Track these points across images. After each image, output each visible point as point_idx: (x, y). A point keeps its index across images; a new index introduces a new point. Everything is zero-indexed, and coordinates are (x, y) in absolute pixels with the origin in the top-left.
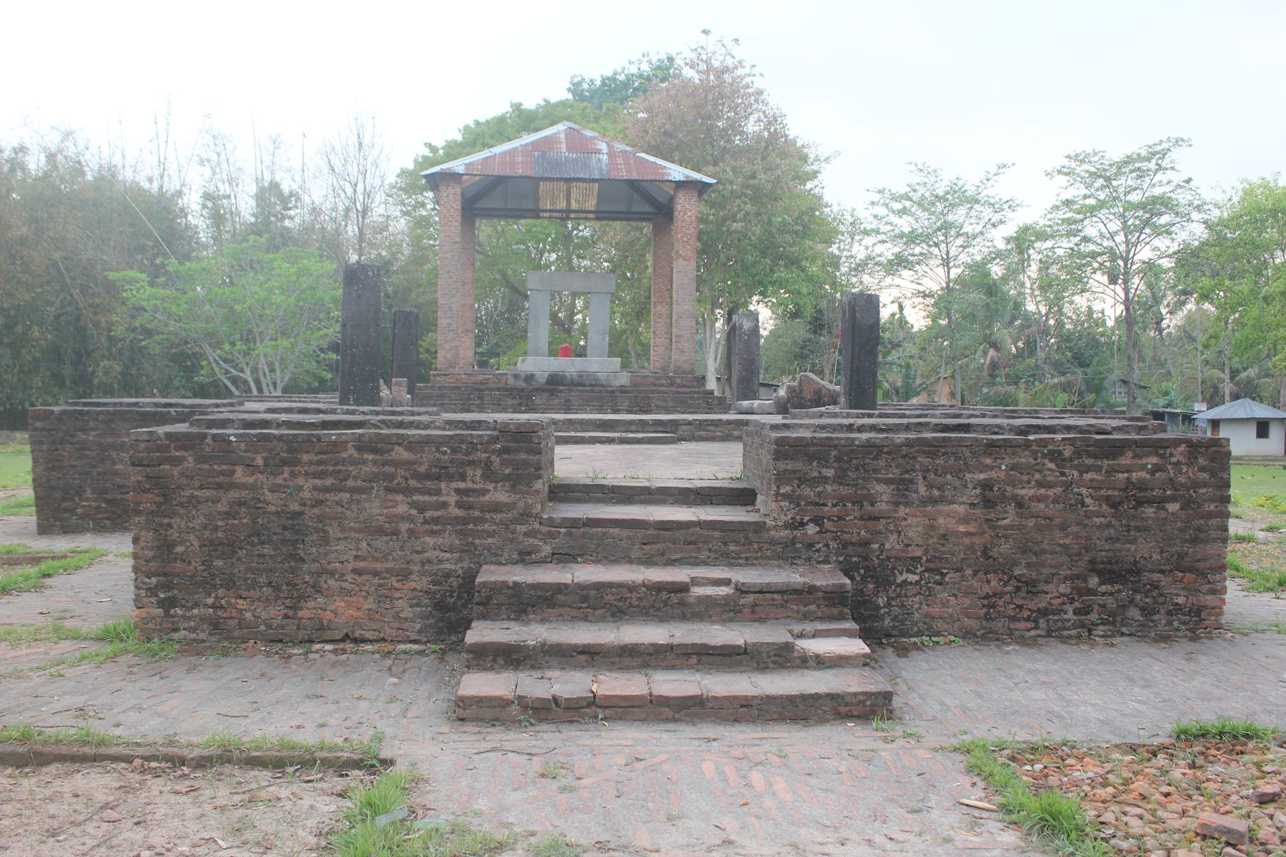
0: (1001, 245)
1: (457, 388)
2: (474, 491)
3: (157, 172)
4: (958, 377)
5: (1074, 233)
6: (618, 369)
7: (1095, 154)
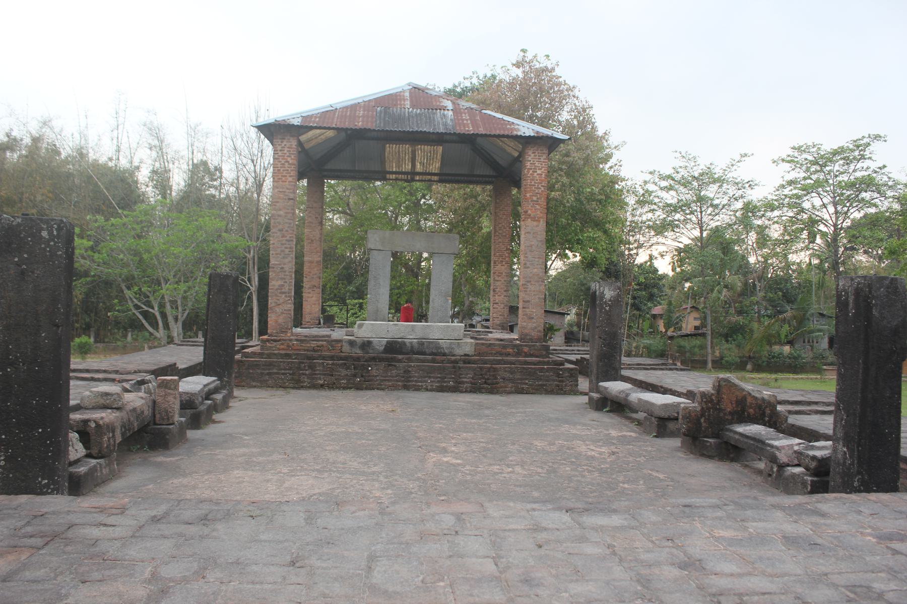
1: (288, 356)
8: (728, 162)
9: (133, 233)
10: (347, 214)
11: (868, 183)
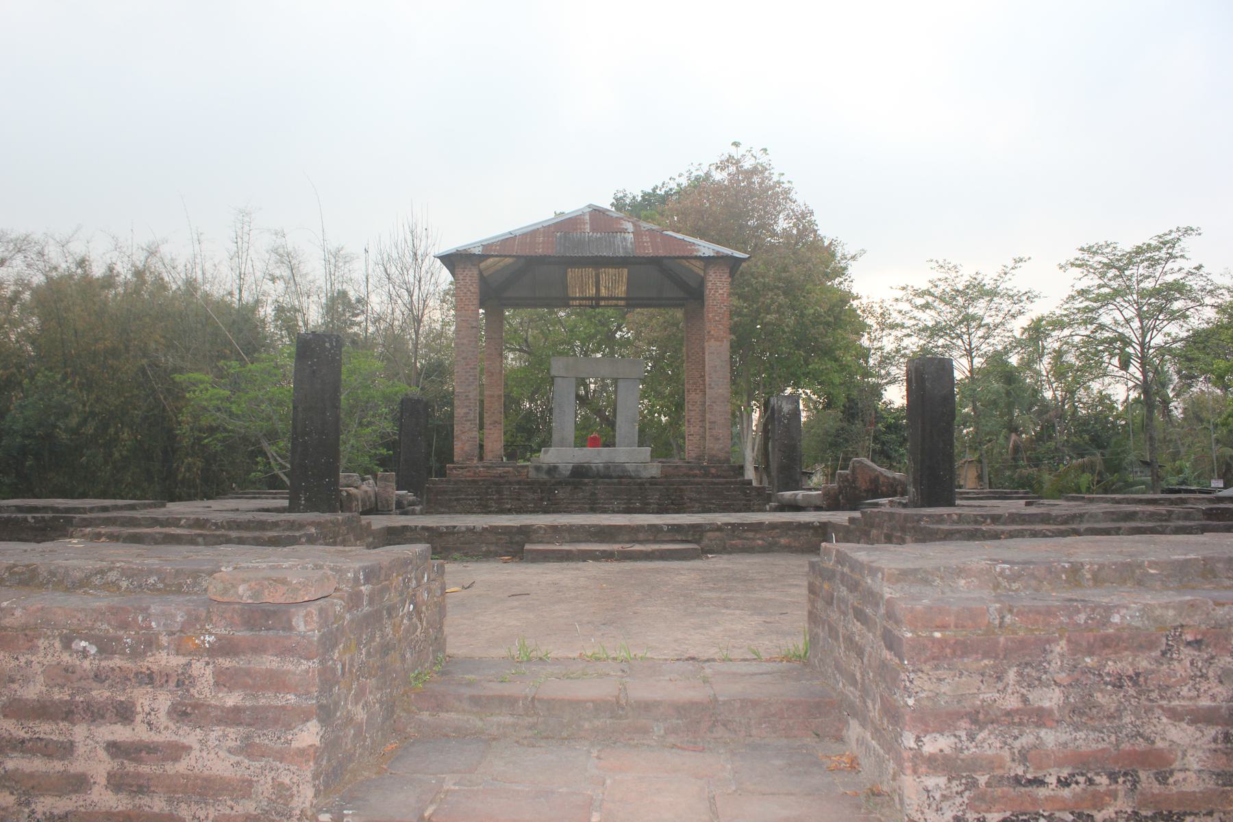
0: (1017, 334)
1: (474, 481)
2: (151, 749)
3: (235, 287)
4: (985, 461)
5: (1091, 321)
6: (649, 459)
7: (1108, 246)
8: (1000, 269)
10: (525, 352)
11: (1178, 288)
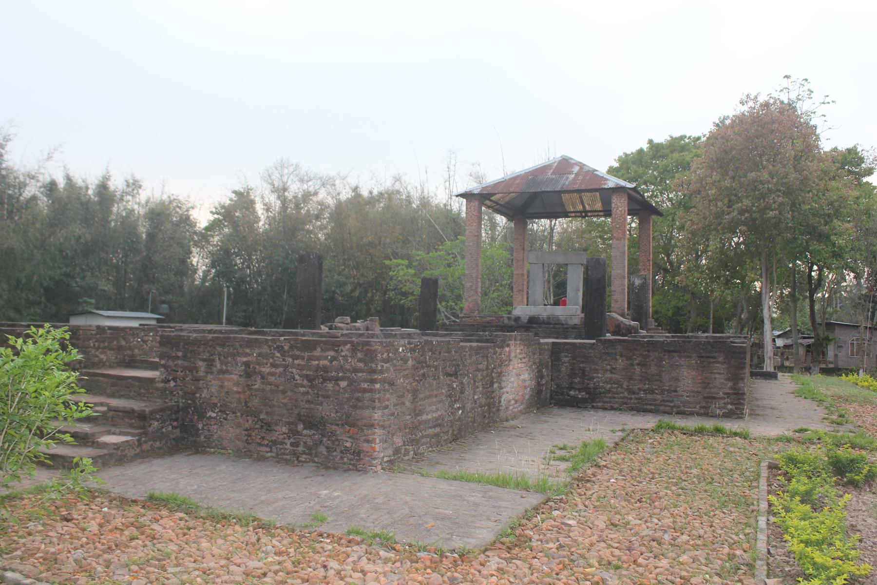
9: (445, 263)
